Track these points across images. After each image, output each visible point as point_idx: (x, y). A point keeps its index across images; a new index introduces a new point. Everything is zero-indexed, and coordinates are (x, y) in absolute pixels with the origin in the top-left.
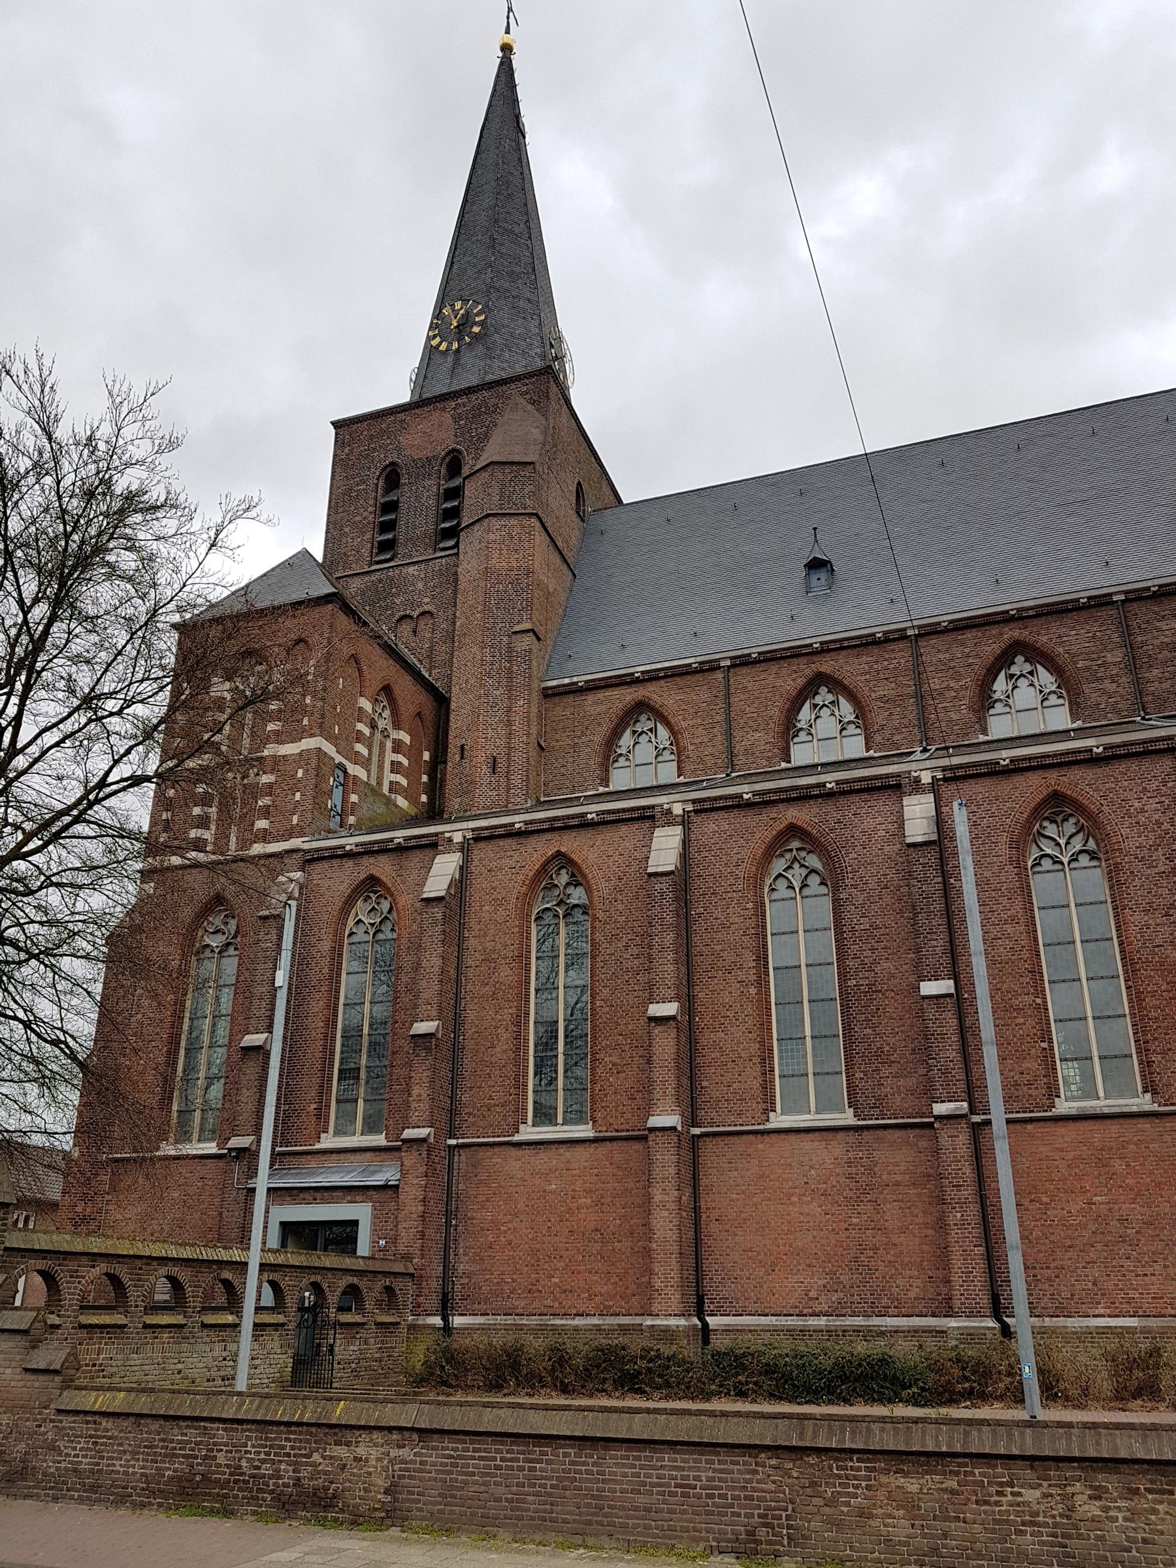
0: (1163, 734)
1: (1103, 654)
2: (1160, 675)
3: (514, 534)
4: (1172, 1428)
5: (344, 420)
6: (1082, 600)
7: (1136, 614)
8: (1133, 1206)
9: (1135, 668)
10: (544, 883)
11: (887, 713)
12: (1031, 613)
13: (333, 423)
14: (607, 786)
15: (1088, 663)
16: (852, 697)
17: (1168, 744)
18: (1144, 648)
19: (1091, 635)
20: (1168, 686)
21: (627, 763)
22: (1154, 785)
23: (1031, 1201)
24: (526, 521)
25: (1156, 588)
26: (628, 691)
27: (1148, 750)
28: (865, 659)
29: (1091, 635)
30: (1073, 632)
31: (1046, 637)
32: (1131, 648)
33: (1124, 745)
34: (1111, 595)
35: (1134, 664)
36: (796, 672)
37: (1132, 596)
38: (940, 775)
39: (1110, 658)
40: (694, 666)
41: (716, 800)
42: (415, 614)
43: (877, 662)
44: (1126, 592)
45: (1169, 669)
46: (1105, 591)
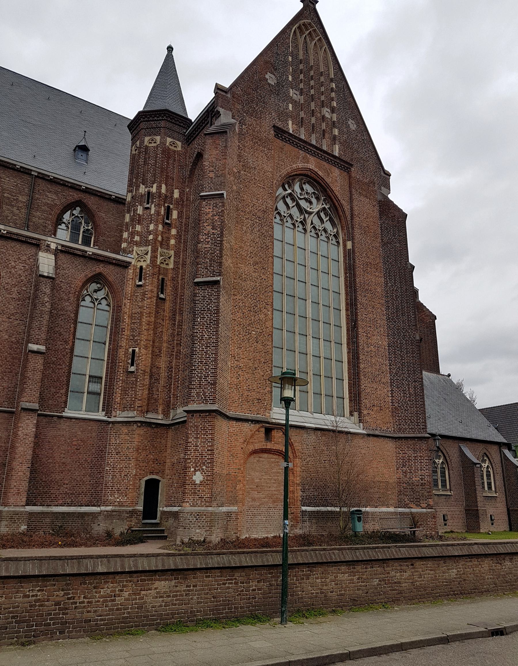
0: (36, 237)
1: (18, 195)
2: (40, 216)
4: (517, 543)
6: (17, 166)
7: (39, 185)
9: (30, 208)
15: (9, 196)
17: (37, 242)
18: (38, 201)
19: (15, 184)
20: (42, 222)
22: (24, 258)
25: (52, 178)
27: (27, 241)
29: (15, 184)
32: (32, 198)
33: (17, 234)
34: (31, 170)
35: (30, 206)
37: (40, 176)
39: (20, 198)
44: (39, 173)
45: (45, 215)
46: (29, 167)
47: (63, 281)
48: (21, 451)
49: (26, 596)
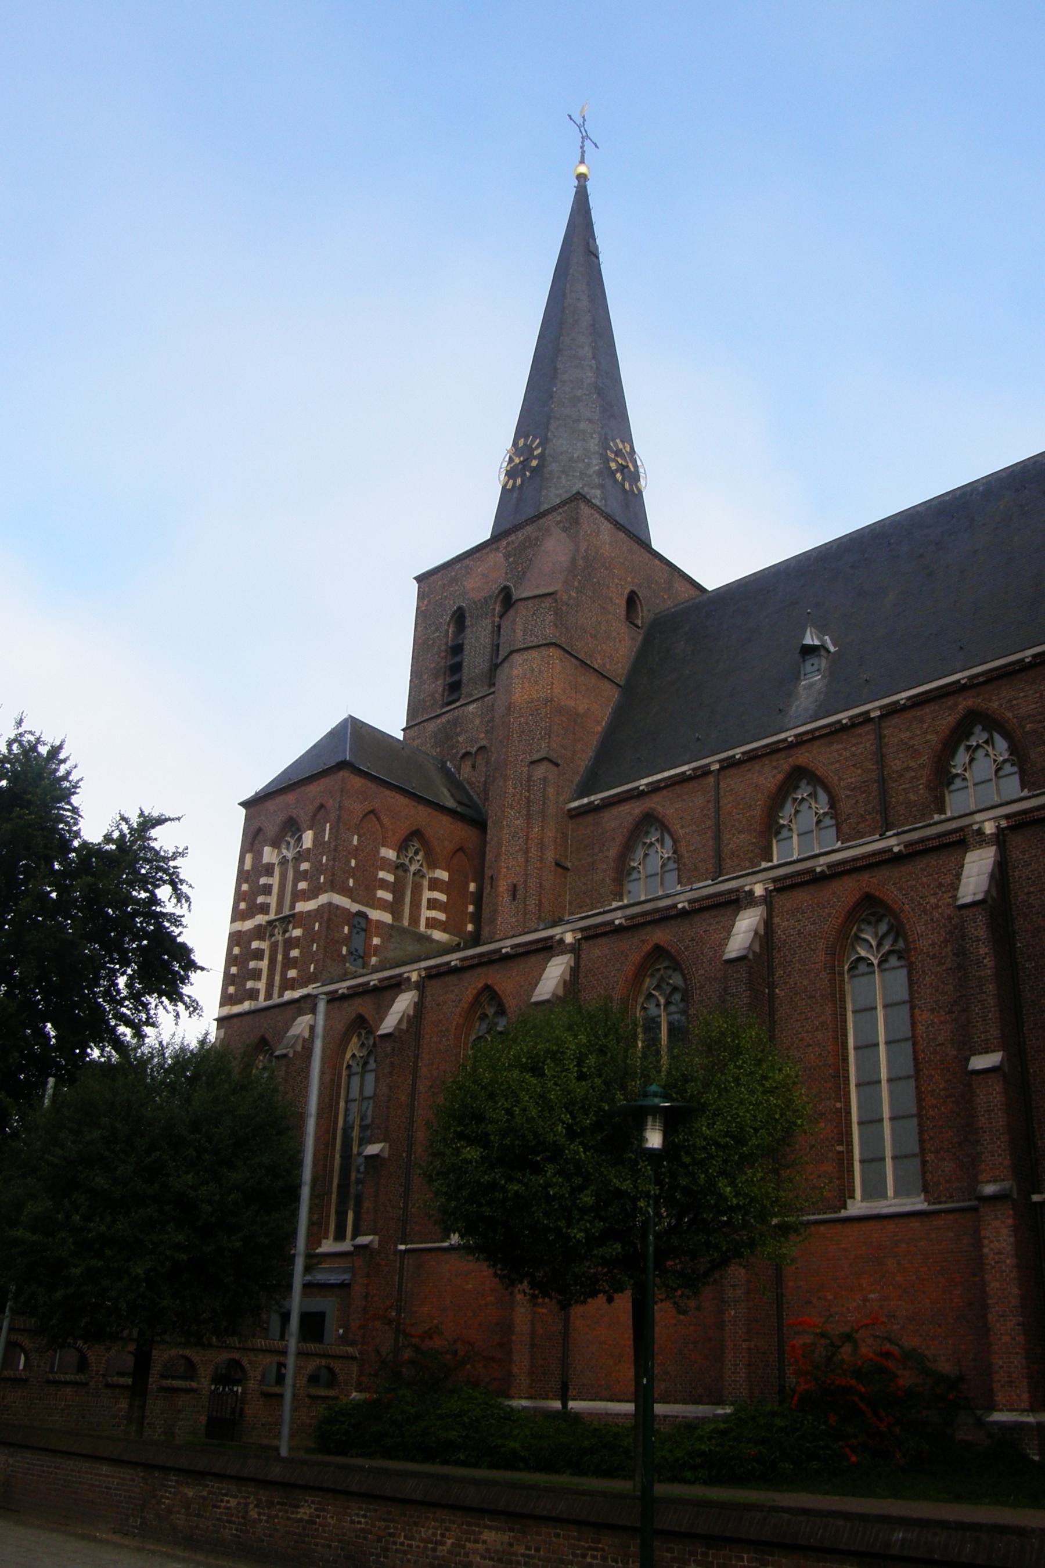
3: (534, 666)
5: (424, 574)
8: (900, 1302)
10: (479, 1013)
11: (854, 801)
12: (981, 679)
13: (415, 578)
14: (621, 900)
16: (1007, 735)
17: (960, 836)
21: (964, 784)
23: (819, 1298)
24: (544, 652)
26: (638, 804)
28: (835, 747)
30: (1022, 695)
31: (997, 703)
36: (775, 768)
38: (579, 936)
40: (688, 773)
41: (598, 927)
42: (474, 749)
43: (846, 749)
47: (1032, 889)
48: (997, 1289)
49: (352, 1522)
